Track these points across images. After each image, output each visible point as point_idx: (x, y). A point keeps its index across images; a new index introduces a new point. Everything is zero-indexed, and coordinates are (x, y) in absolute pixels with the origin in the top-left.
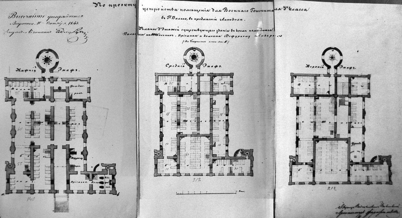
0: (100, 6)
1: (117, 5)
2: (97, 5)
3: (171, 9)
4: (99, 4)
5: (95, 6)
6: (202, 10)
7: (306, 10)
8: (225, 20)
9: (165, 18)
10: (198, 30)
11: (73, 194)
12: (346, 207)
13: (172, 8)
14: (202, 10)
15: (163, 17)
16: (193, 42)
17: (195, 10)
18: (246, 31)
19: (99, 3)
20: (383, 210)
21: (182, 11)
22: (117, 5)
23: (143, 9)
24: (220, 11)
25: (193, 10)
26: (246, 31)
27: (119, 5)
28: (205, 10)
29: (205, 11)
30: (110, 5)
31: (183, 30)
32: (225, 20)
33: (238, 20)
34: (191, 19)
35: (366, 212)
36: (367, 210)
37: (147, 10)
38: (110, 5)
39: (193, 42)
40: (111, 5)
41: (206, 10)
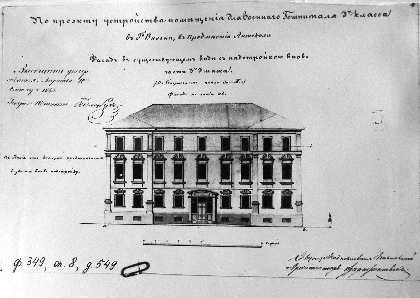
0: (41, 23)
1: (129, 21)
2: (36, 20)
3: (153, 19)
4: (39, 20)
5: (34, 23)
6: (210, 19)
7: (385, 15)
8: (243, 36)
9: (132, 39)
10: (163, 60)
11: (126, 208)
12: (310, 257)
13: (156, 17)
14: (210, 19)
15: (130, 36)
16: (171, 83)
17: (115, 20)
18: (194, 60)
19: (38, 18)
20: (297, 265)
21: (172, 22)
22: (128, 21)
23: (105, 20)
24: (222, 18)
25: (192, 20)
26: (194, 60)
27: (379, 15)
28: (217, 18)
29: (217, 20)
30: (170, 20)
31: (136, 61)
33: (158, 39)
34: (182, 38)
35: (344, 267)
36: (346, 264)
37: (111, 22)
38: (170, 20)
39: (171, 83)
40: (56, 21)
41: (219, 17)
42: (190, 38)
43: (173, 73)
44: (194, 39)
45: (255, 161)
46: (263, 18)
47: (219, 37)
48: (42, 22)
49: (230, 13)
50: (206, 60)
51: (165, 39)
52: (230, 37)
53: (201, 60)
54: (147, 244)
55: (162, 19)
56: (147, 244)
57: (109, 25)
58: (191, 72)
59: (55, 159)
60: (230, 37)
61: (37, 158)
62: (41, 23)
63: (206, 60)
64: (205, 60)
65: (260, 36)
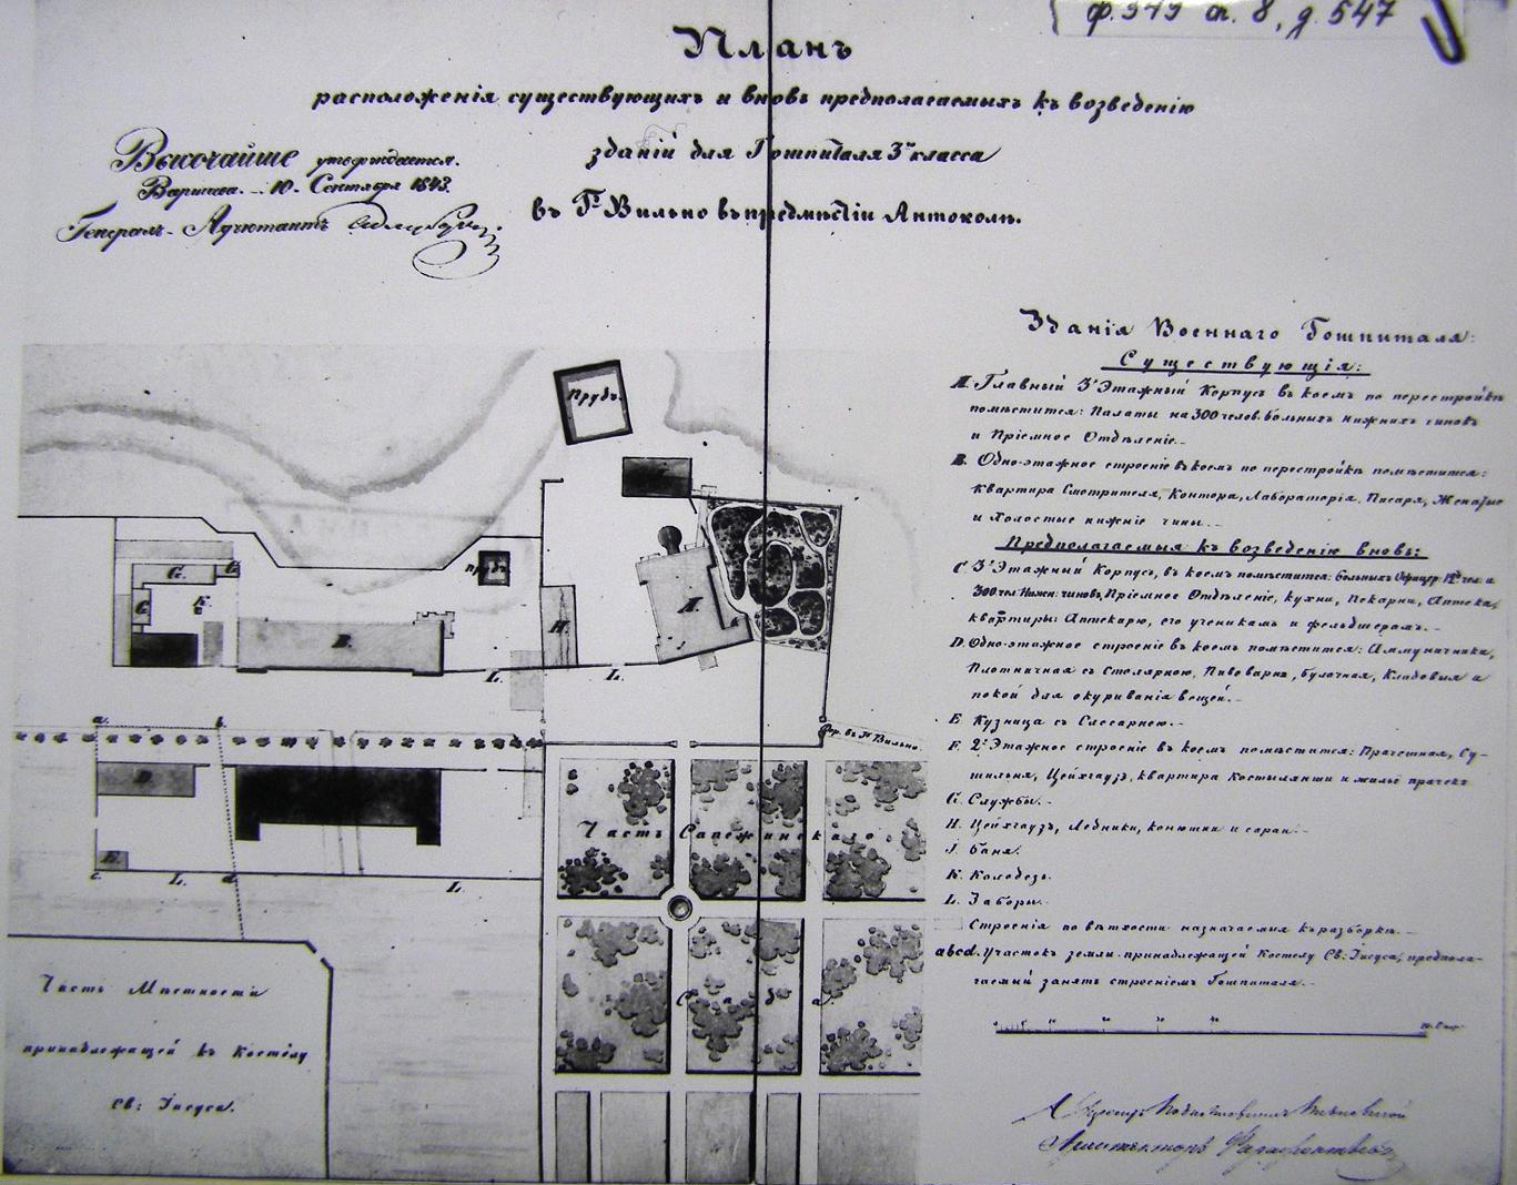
0: (724, 53)
32: (1194, 777)
42: (1000, 437)
43: (679, 211)
44: (320, 104)
45: (156, 574)
46: (816, 48)
47: (266, 1053)
48: (729, 49)
49: (720, 27)
50: (1230, 331)
51: (460, 101)
52: (670, 157)
53: (721, 218)
54: (1007, 1032)
55: (793, 40)
56: (1007, 1032)
57: (1361, 28)
58: (1032, 328)
59: (1223, 394)
60: (670, 157)
61: (1347, 395)
62: (724, 53)
63: (1230, 331)
64: (1339, 339)
65: (1309, 470)
